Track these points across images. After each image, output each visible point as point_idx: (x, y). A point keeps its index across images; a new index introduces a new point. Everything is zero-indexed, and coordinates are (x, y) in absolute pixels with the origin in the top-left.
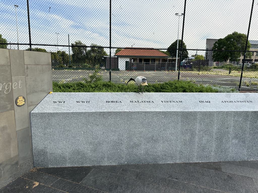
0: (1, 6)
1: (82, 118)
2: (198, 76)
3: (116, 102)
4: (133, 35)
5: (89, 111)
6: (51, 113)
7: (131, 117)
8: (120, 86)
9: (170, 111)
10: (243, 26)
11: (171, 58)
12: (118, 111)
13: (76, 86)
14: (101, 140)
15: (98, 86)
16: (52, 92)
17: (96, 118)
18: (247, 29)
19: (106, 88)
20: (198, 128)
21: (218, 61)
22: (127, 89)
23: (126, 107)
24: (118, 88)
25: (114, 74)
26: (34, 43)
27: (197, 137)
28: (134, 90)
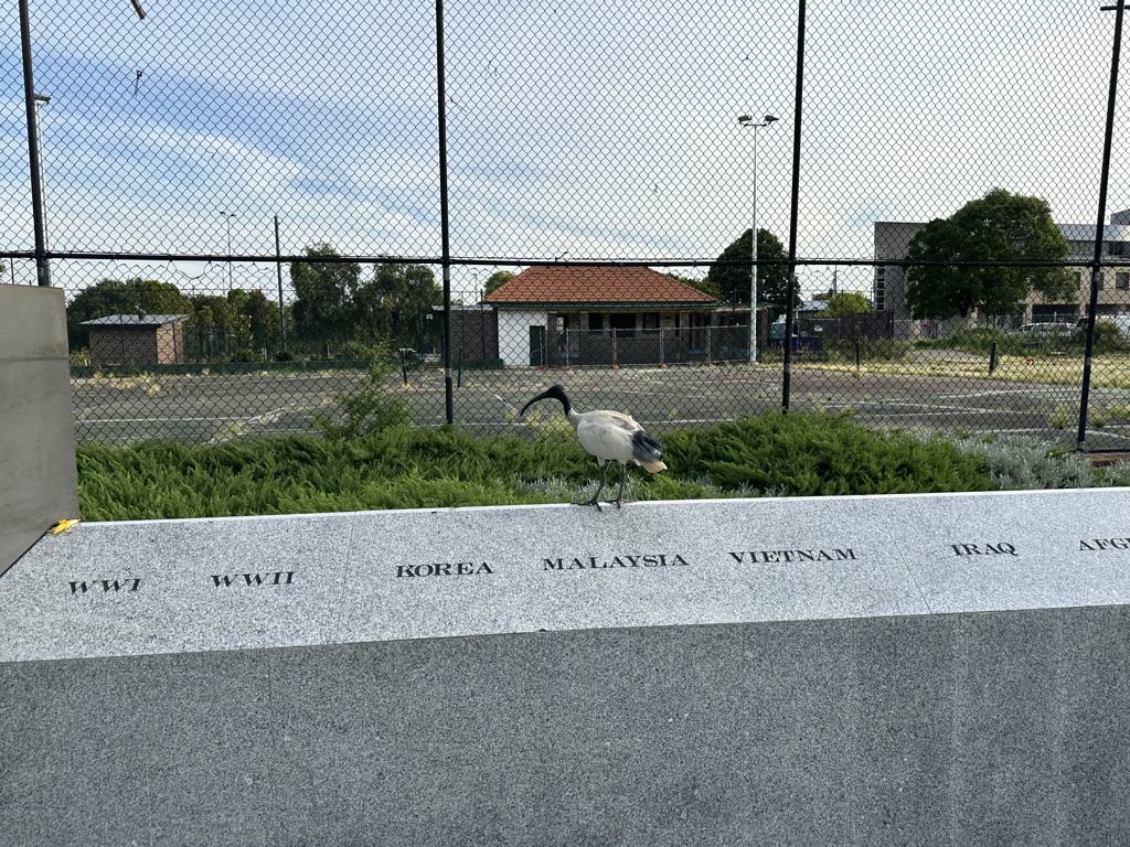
0: (6, 112)
1: (241, 689)
2: (855, 385)
3: (460, 572)
4: (563, 214)
5: (288, 643)
6: (43, 666)
7: (550, 666)
8: (498, 448)
9: (792, 619)
10: (1077, 144)
11: (728, 310)
12: (469, 632)
13: (269, 457)
14: (368, 820)
15: (383, 452)
16: (76, 521)
17: (328, 683)
18: (1096, 161)
19: (429, 463)
20: (959, 712)
21: (931, 316)
22: (535, 461)
23: (517, 599)
24: (488, 461)
25: (475, 388)
26: (60, 249)
27: (954, 770)
28: (569, 467)
